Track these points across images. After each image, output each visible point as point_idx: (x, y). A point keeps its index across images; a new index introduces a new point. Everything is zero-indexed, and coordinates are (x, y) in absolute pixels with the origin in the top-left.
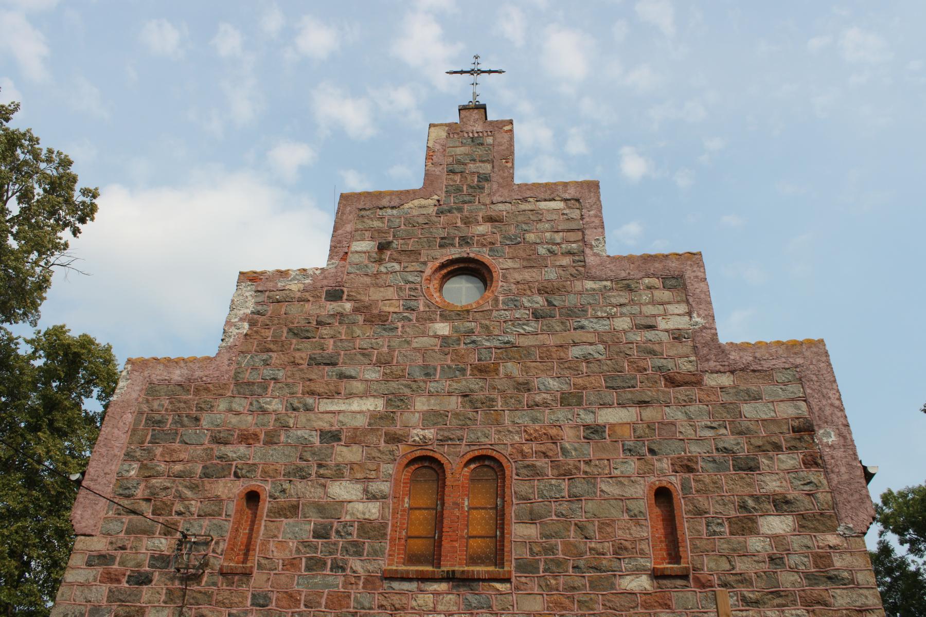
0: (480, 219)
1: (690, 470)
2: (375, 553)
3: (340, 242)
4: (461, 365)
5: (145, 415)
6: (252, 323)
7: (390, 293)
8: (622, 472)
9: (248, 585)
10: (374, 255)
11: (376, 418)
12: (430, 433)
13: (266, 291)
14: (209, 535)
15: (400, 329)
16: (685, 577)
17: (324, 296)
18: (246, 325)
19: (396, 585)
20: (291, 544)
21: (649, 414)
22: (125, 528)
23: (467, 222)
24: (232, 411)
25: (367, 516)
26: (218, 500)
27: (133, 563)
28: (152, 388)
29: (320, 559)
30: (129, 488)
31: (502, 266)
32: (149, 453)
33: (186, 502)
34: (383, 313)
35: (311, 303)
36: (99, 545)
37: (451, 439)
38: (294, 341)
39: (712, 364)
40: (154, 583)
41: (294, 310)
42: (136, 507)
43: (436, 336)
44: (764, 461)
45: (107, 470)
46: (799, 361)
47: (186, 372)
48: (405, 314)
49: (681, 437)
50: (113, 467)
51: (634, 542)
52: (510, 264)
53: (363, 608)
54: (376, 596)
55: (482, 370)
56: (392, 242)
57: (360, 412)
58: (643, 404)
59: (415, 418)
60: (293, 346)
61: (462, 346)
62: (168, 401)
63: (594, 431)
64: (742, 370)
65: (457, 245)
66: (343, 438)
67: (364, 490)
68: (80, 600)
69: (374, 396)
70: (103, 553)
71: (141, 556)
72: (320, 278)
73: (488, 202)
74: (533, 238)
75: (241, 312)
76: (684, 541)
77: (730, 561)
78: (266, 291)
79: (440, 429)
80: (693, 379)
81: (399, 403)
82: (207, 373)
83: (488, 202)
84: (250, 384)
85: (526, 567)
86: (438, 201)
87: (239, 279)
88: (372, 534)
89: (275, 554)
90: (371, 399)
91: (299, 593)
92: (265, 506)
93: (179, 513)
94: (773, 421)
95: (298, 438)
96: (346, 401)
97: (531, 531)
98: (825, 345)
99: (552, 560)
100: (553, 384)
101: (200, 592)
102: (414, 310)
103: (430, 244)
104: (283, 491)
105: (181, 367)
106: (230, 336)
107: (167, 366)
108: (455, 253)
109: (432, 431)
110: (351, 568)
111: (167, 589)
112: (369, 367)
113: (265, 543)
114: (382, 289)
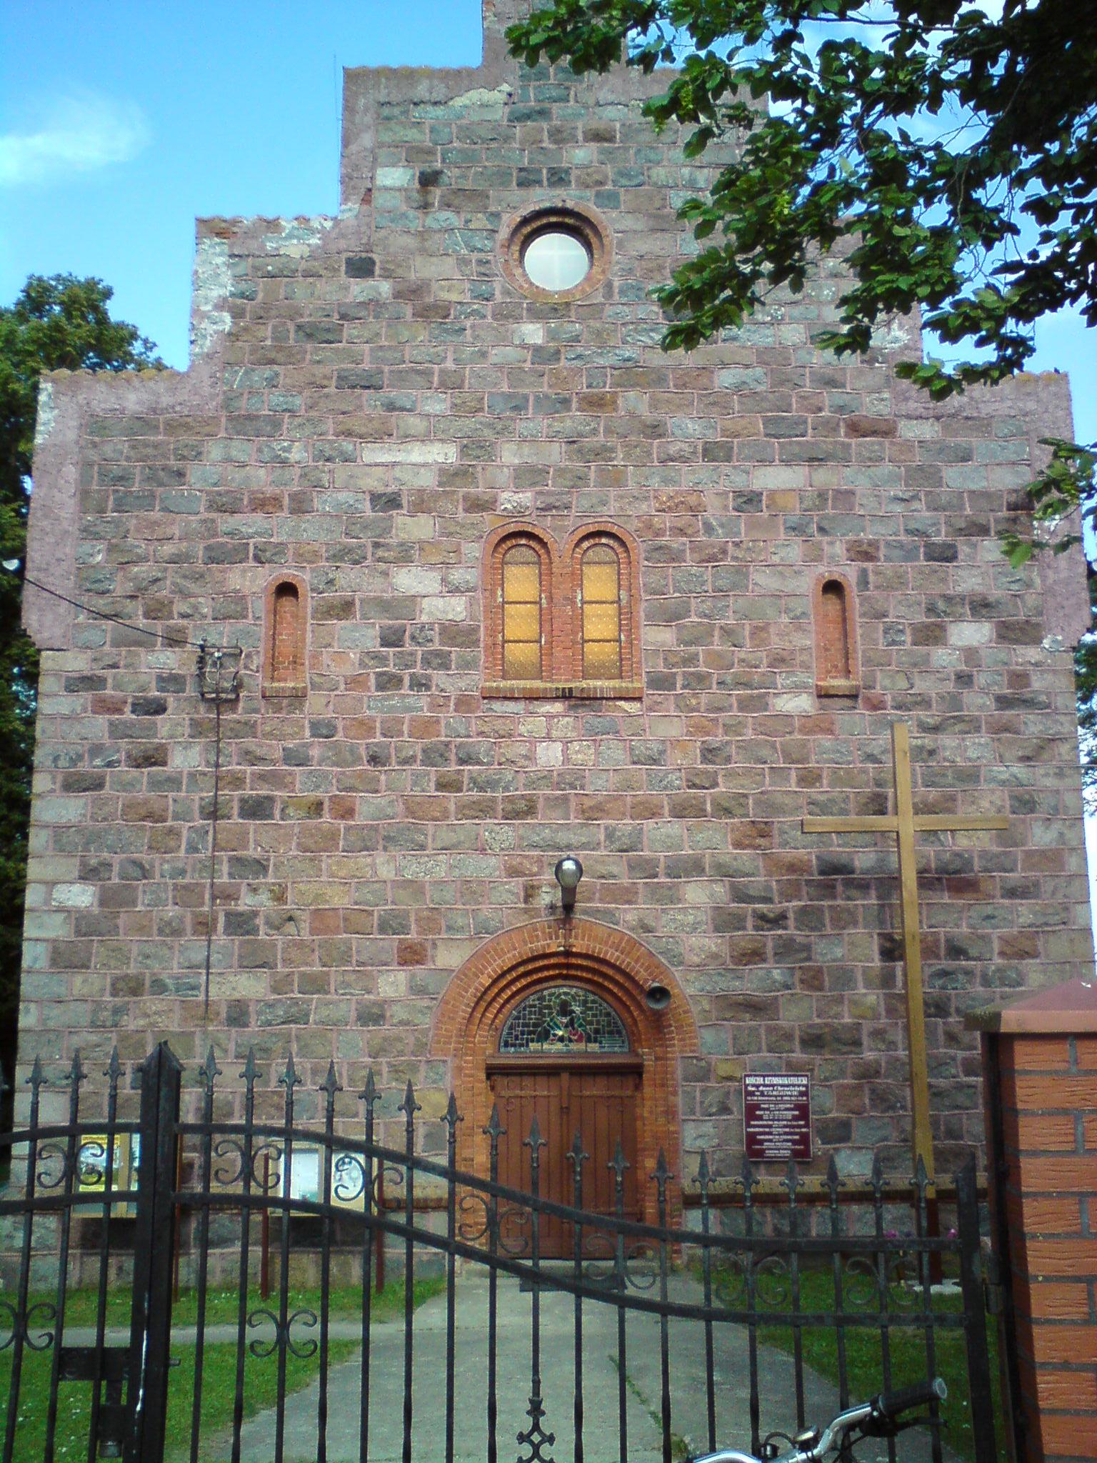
0: (580, 137)
1: (868, 557)
2: (467, 665)
3: (356, 167)
4: (566, 394)
5: (96, 468)
6: (237, 314)
7: (448, 266)
8: (782, 559)
9: (302, 711)
10: (415, 195)
11: (451, 476)
12: (526, 497)
13: (248, 256)
14: (236, 647)
15: (468, 332)
16: (854, 697)
17: (343, 268)
18: (227, 317)
19: (498, 706)
20: (352, 655)
21: (825, 477)
22: (108, 640)
23: (558, 136)
24: (232, 461)
25: (450, 617)
26: (240, 598)
27: (133, 687)
28: (96, 422)
29: (394, 676)
30: (100, 581)
31: (617, 226)
32: (117, 527)
33: (192, 600)
34: (441, 303)
35: (324, 280)
36: (77, 663)
37: (555, 507)
38: (309, 346)
39: (912, 405)
40: (169, 711)
41: (300, 290)
42: (118, 608)
43: (524, 346)
44: (963, 550)
45: (59, 555)
46: (1031, 405)
47: (145, 396)
48: (475, 307)
49: (861, 513)
50: (68, 550)
51: (792, 652)
52: (629, 222)
53: (458, 736)
54: (473, 720)
55: (595, 403)
56: (442, 172)
57: (424, 465)
58: (815, 460)
59: (504, 476)
60: (308, 357)
61: (563, 362)
62: (126, 445)
63: (749, 500)
64: (953, 416)
65: (545, 183)
66: (404, 502)
67: (443, 580)
68: (73, 737)
69: (442, 441)
70: (86, 673)
71: (143, 678)
72: (333, 235)
73: (591, 102)
74: (663, 177)
75: (216, 293)
76: (855, 651)
77: (908, 679)
78: (248, 256)
79: (540, 493)
80: (884, 427)
81: (479, 452)
82: (181, 399)
83: (591, 102)
84: (250, 418)
85: (661, 682)
86: (510, 95)
87: (198, 233)
88: (460, 640)
89: (333, 669)
90: (438, 445)
91: (373, 719)
92: (309, 601)
93: (184, 616)
94: (985, 495)
95: (340, 504)
96: (402, 447)
97: (664, 636)
98: (1068, 383)
99: (692, 674)
100: (692, 427)
101: (239, 722)
102: (487, 300)
103: (502, 177)
104: (331, 582)
105: (135, 389)
106: (204, 337)
107: (112, 387)
108: (541, 198)
109: (529, 494)
110: (437, 685)
111: (191, 719)
112: (429, 393)
113: (316, 656)
114: (434, 260)
